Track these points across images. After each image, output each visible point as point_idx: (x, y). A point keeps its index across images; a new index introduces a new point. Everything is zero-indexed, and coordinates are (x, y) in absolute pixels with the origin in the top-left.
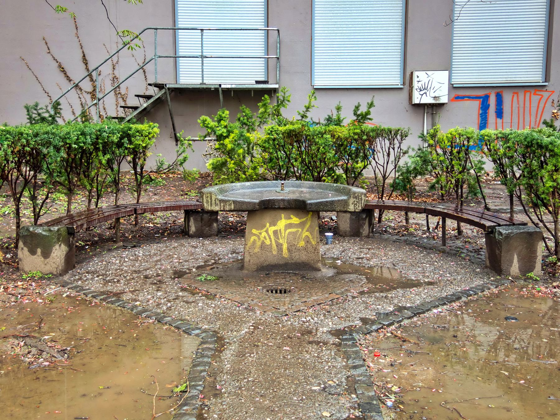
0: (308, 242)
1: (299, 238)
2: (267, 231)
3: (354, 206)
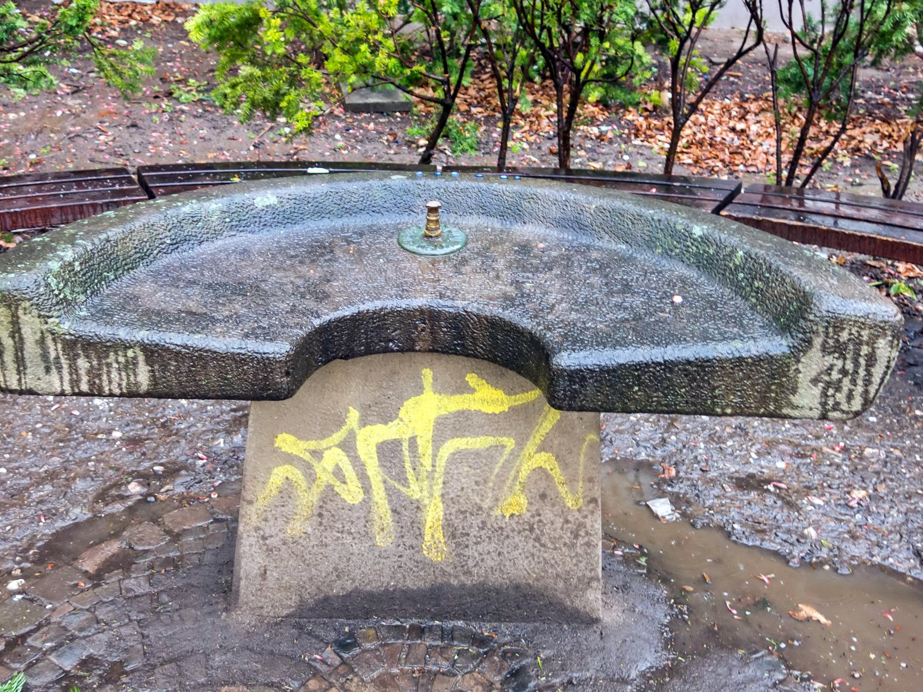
0: (543, 496)
1: (501, 479)
2: (348, 446)
3: (824, 394)
